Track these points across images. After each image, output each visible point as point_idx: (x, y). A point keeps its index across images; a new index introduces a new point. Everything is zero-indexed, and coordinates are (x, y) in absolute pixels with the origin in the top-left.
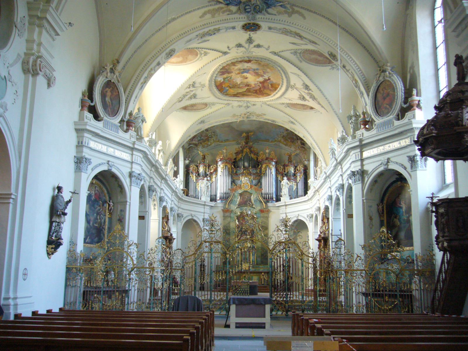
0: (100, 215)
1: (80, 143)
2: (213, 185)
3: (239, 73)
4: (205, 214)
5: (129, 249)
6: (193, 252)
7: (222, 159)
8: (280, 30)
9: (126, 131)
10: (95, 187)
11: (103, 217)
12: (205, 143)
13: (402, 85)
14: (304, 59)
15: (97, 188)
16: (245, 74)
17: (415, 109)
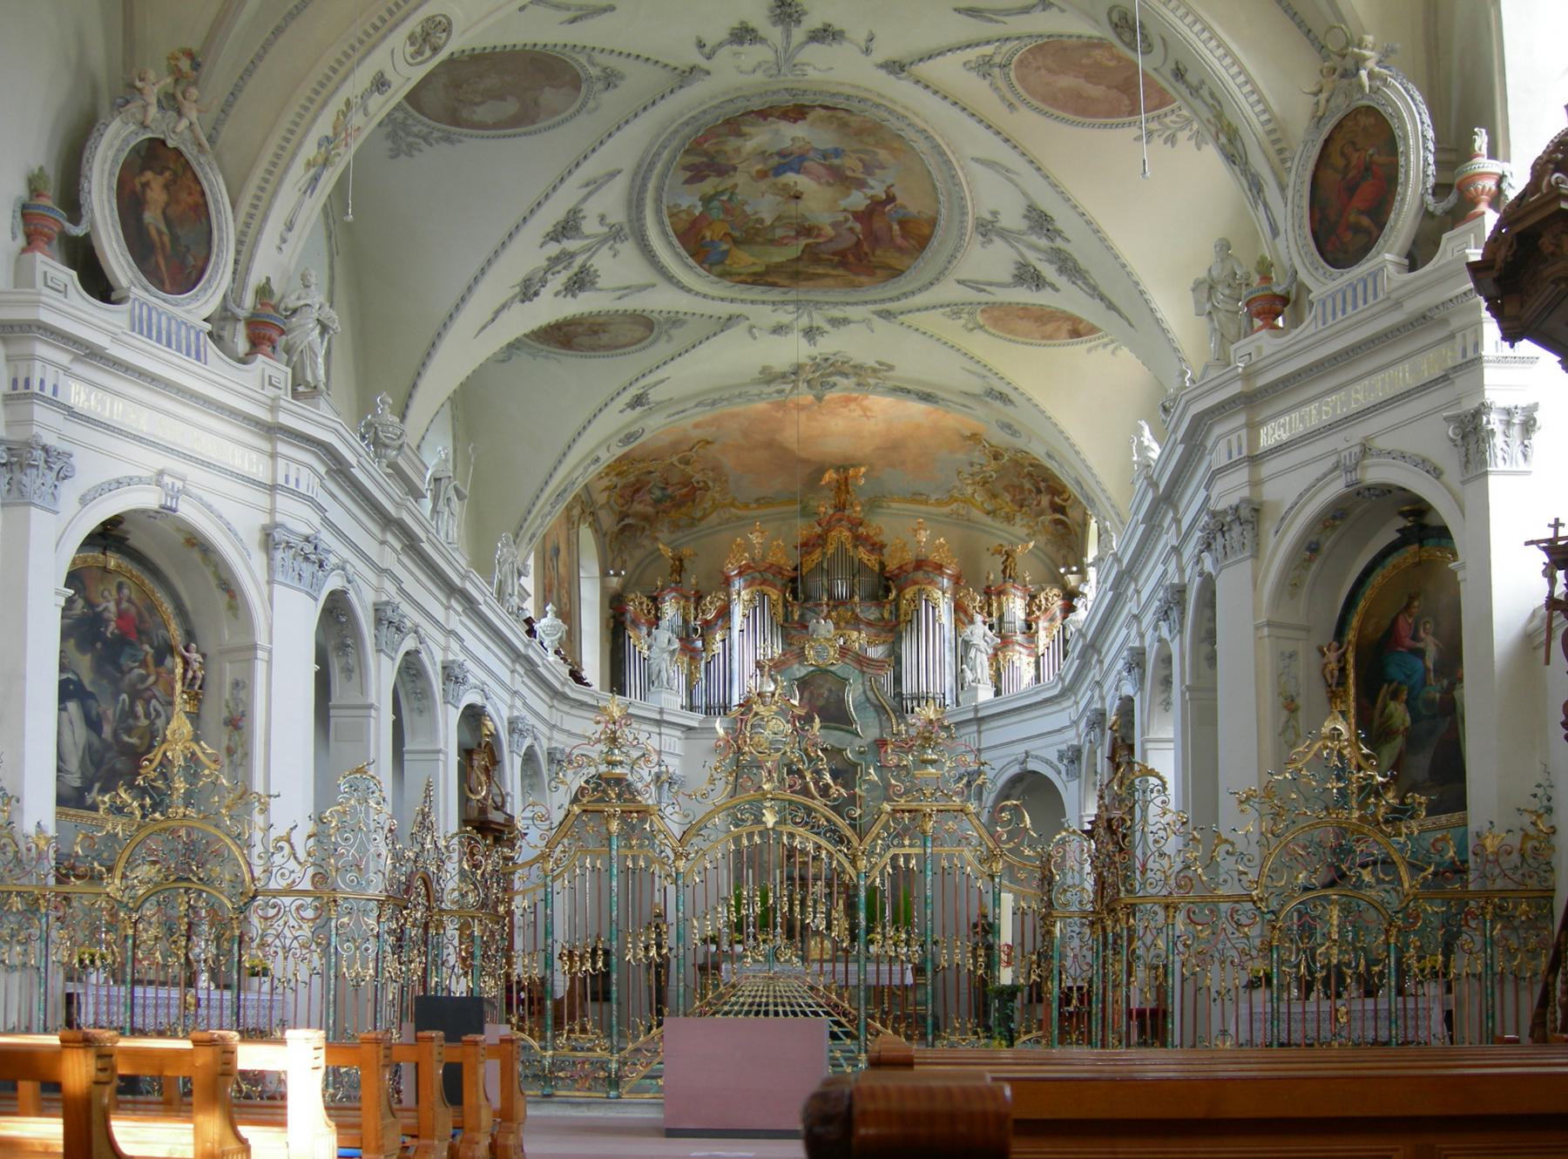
0: (148, 702)
1: (21, 383)
3: (763, 175)
6: (538, 852)
7: (748, 567)
10: (120, 587)
11: (160, 708)
12: (683, 509)
13: (1427, 120)
14: (1025, 95)
15: (126, 591)
16: (790, 178)
17: (1483, 213)
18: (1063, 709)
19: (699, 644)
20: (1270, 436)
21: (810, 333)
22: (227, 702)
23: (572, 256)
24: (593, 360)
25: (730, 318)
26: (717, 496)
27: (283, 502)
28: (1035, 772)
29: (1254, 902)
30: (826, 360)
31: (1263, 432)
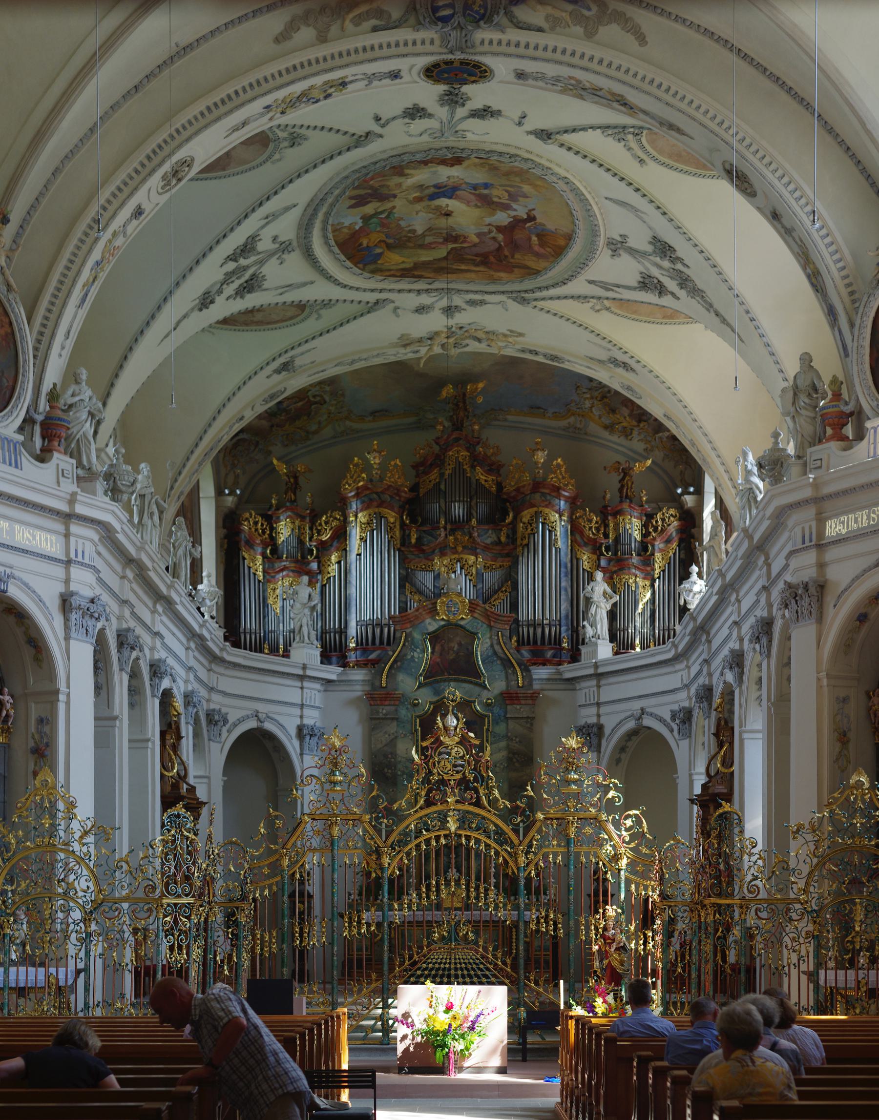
2: (333, 590)
3: (419, 200)
4: (306, 712)
5: (84, 844)
7: (365, 488)
8: (559, 81)
9: (43, 457)
14: (654, 153)
16: (443, 202)
18: (676, 672)
19: (314, 566)
20: (834, 528)
21: (449, 311)
22: (33, 735)
23: (245, 268)
24: (245, 333)
25: (377, 303)
26: (332, 409)
27: (75, 571)
28: (649, 728)
29: (802, 904)
30: (461, 328)
31: (828, 523)
